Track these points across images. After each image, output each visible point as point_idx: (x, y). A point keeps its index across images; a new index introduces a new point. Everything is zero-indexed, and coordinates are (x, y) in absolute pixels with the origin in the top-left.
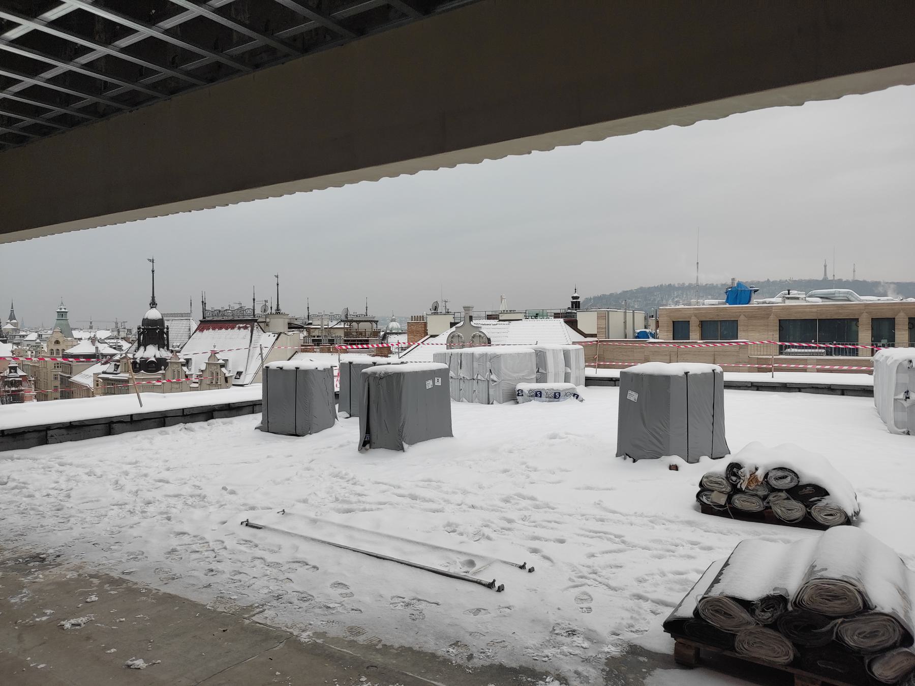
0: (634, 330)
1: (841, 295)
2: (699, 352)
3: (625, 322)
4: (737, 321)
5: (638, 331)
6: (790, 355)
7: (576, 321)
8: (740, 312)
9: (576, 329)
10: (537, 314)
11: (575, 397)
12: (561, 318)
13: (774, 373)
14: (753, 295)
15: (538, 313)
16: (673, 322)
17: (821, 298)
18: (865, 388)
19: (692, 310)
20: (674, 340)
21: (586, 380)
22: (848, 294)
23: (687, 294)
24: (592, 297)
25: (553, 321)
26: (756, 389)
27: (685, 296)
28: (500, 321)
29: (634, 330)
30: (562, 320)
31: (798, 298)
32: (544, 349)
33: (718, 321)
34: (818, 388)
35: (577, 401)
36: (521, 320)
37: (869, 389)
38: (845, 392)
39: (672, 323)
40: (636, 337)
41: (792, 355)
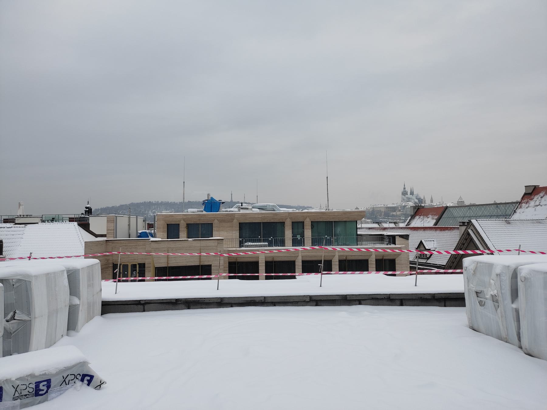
0: (137, 231)
1: (270, 207)
2: (190, 247)
3: (129, 225)
4: (212, 223)
5: (140, 232)
6: (247, 247)
7: (88, 224)
8: (214, 217)
9: (88, 231)
10: (53, 219)
11: (86, 382)
12: (75, 222)
13: (74, 217)
14: (221, 205)
15: (54, 217)
16: (167, 224)
17: (259, 209)
18: (422, 296)
19: (182, 216)
20: (168, 239)
21: (102, 305)
22: (274, 206)
23: (160, 208)
24: (100, 208)
25: (56, 225)
26: (315, 303)
27: (159, 209)
28: (16, 224)
29: (137, 231)
30: (76, 223)
31: (247, 209)
32: (29, 276)
33: (199, 224)
34: (378, 299)
35: (90, 390)
36: (38, 223)
37: (425, 297)
38: (404, 301)
39: (166, 225)
40: (139, 237)
41: (249, 247)
